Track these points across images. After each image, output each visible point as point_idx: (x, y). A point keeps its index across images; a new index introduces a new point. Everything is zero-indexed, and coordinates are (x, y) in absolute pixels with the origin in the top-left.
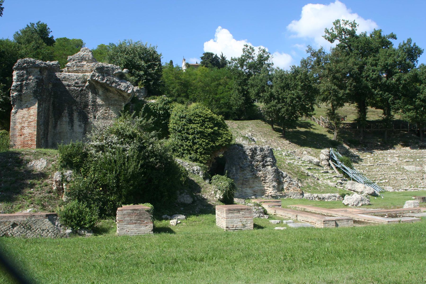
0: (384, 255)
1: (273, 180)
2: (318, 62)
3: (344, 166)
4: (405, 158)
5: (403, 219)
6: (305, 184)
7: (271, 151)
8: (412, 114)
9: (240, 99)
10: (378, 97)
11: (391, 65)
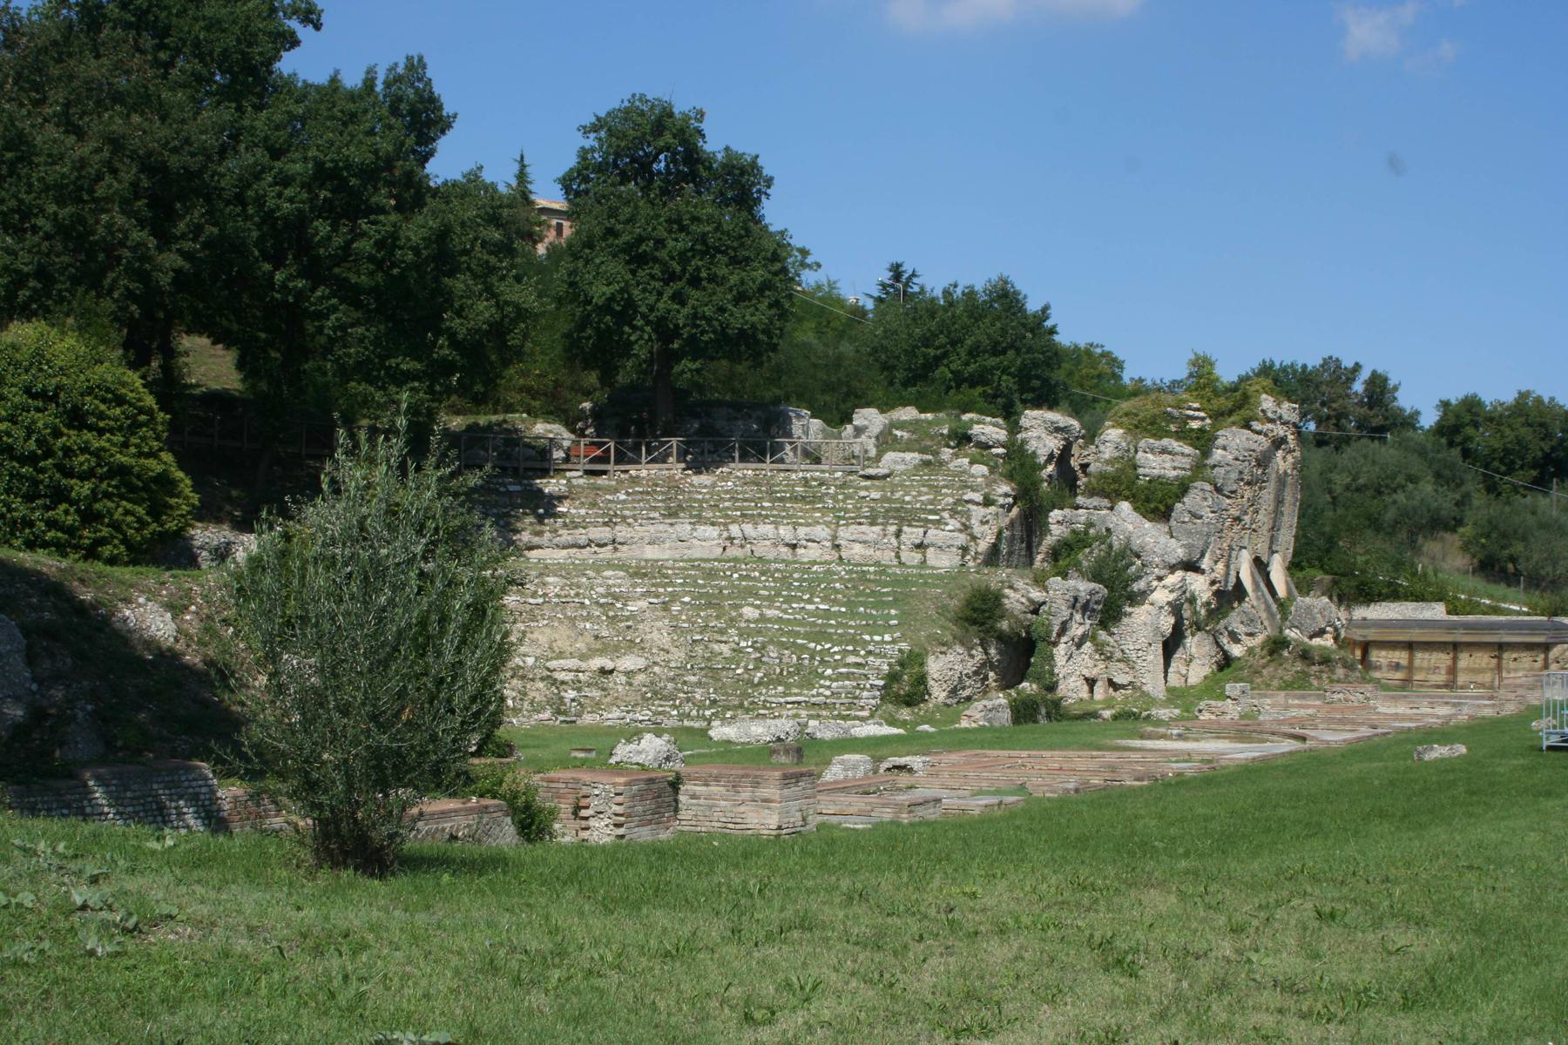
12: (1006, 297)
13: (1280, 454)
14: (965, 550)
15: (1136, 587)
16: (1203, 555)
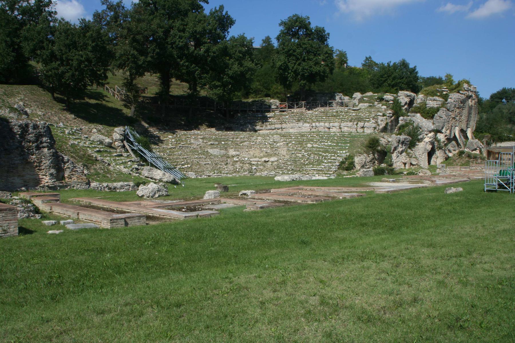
0: (171, 265)
1: (50, 166)
2: (116, 18)
3: (141, 148)
4: (210, 141)
5: (201, 213)
6: (92, 171)
7: (48, 131)
8: (219, 91)
9: (9, 55)
10: (183, 69)
11: (200, 33)
12: (404, 64)
13: (470, 100)
14: (375, 128)
15: (420, 137)
16: (442, 128)
